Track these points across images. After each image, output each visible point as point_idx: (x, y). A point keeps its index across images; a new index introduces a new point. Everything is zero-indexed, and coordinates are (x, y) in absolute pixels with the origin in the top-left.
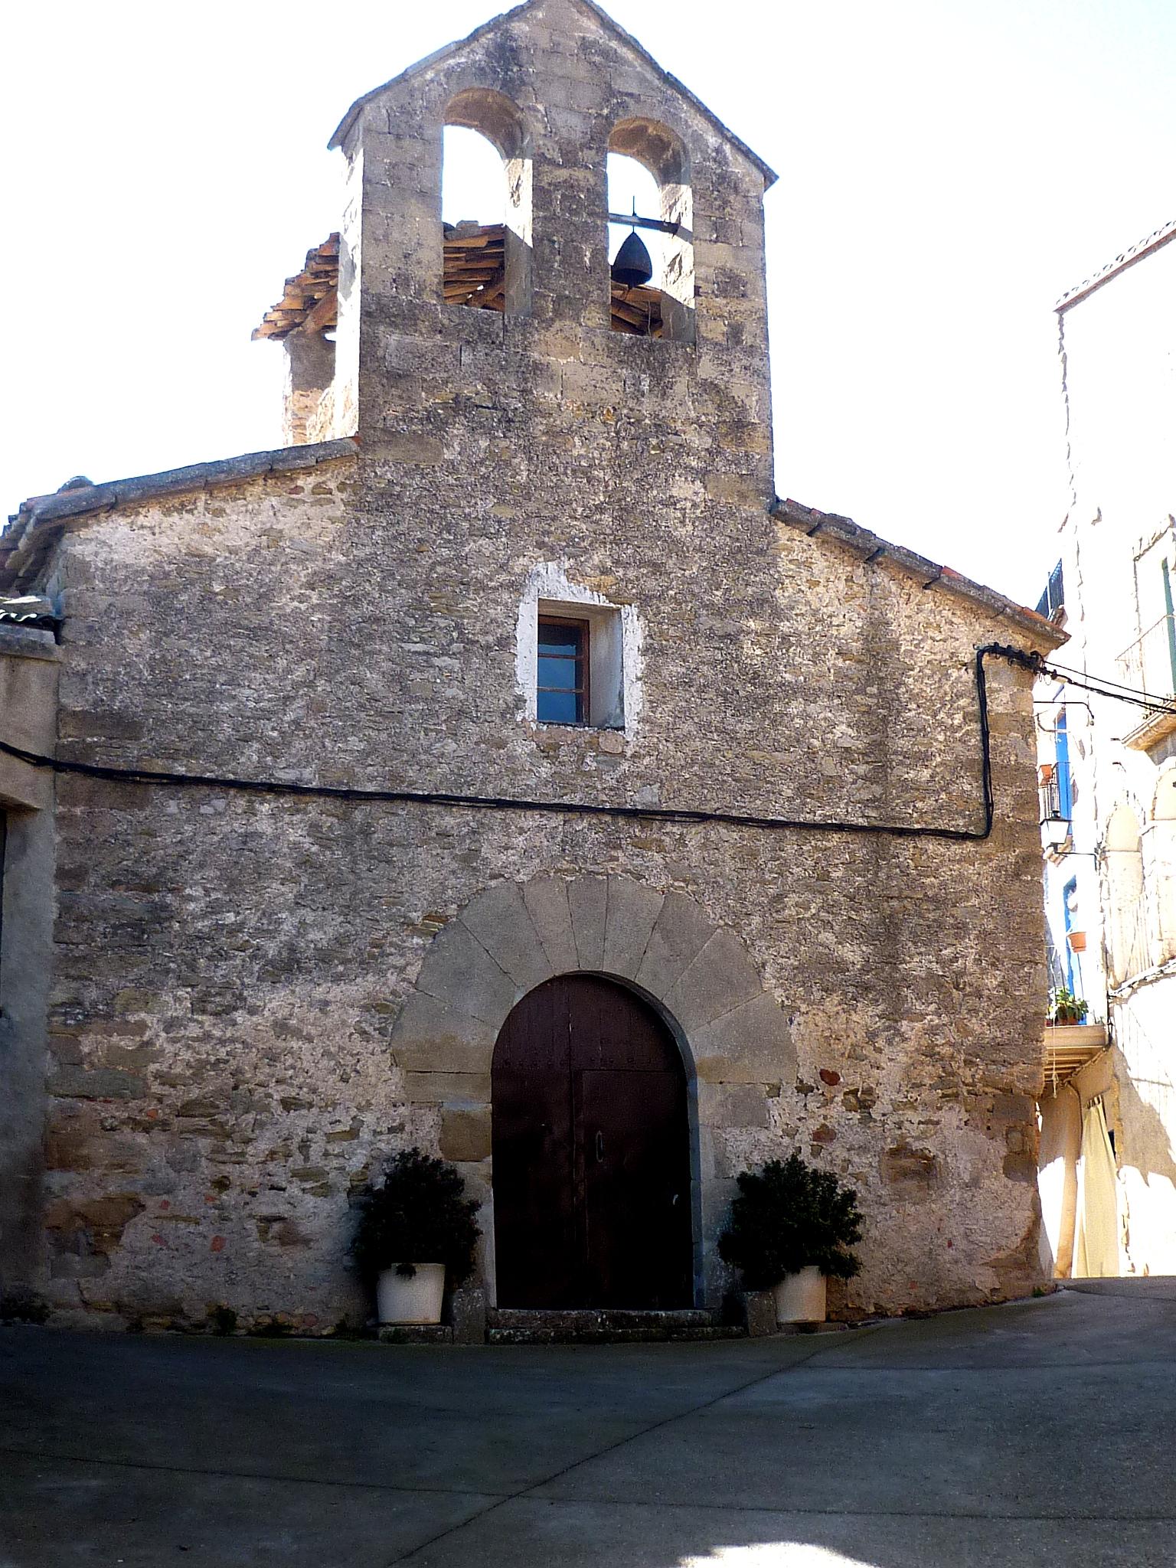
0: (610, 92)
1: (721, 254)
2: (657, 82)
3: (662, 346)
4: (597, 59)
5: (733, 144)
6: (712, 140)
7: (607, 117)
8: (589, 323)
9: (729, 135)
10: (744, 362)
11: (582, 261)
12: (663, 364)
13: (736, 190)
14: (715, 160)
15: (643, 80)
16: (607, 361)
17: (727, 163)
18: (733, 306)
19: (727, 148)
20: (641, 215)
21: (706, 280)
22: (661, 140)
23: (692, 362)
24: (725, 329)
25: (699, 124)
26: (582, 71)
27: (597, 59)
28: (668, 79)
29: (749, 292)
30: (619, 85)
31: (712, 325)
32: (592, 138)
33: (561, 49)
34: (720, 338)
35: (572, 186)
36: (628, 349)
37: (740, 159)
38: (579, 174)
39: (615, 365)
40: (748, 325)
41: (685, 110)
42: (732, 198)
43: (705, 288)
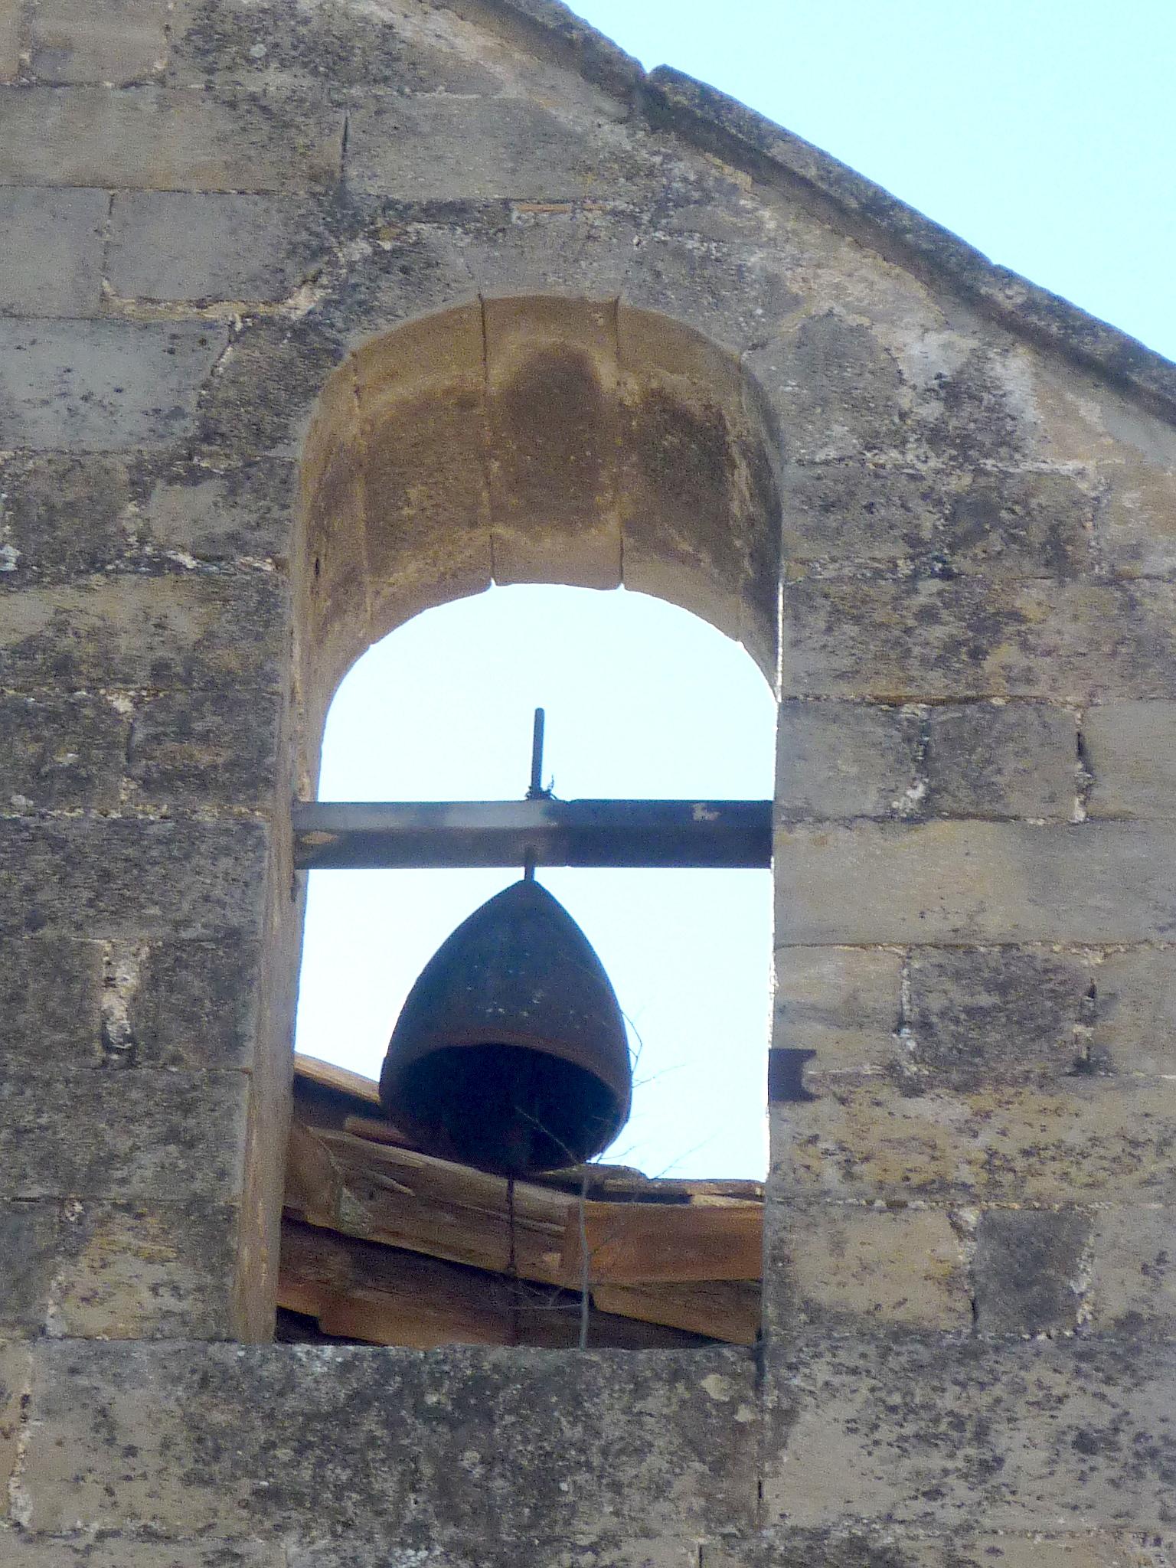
0: (339, 209)
1: (961, 878)
2: (614, 136)
3: (535, 1389)
4: (276, 81)
5: (1041, 343)
6: (925, 345)
7: (301, 331)
8: (95, 1319)
9: (1008, 299)
10: (1080, 1411)
11: (81, 1007)
12: (541, 1485)
13: (1058, 556)
14: (935, 436)
15: (531, 136)
16: (179, 1506)
17: (1007, 443)
18: (1019, 1122)
19: (1015, 373)
20: (570, 784)
21: (850, 1015)
22: (680, 419)
23: (727, 1451)
24: (962, 1253)
25: (848, 283)
26: (185, 142)
27: (276, 81)
28: (680, 112)
29: (1122, 1048)
30: (389, 174)
31: (874, 1236)
32: (209, 435)
33: (75, 68)
34: (927, 1304)
35: (64, 666)
36: (324, 1431)
37: (1092, 408)
38: (115, 606)
39: (233, 1520)
40: (1108, 1212)
41: (769, 234)
42: (1029, 599)
43: (834, 1053)
